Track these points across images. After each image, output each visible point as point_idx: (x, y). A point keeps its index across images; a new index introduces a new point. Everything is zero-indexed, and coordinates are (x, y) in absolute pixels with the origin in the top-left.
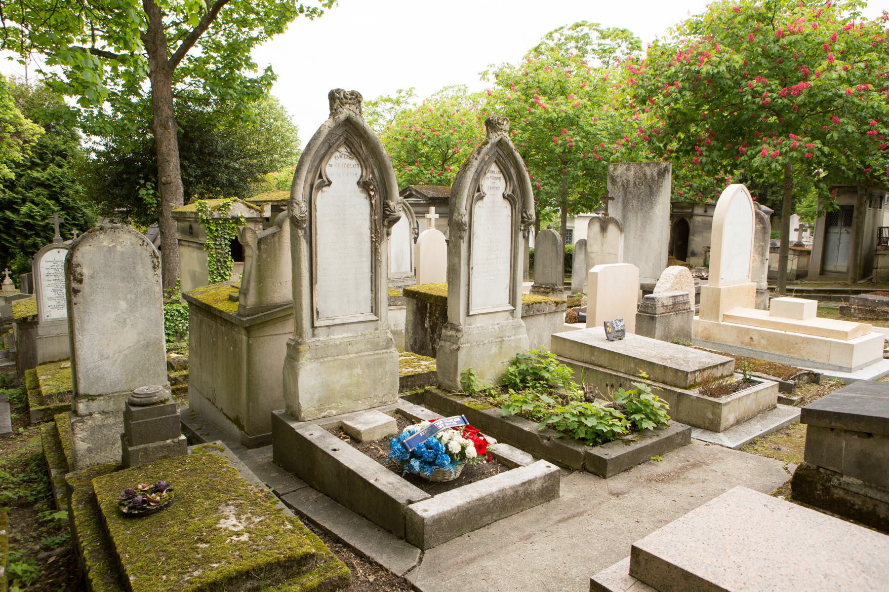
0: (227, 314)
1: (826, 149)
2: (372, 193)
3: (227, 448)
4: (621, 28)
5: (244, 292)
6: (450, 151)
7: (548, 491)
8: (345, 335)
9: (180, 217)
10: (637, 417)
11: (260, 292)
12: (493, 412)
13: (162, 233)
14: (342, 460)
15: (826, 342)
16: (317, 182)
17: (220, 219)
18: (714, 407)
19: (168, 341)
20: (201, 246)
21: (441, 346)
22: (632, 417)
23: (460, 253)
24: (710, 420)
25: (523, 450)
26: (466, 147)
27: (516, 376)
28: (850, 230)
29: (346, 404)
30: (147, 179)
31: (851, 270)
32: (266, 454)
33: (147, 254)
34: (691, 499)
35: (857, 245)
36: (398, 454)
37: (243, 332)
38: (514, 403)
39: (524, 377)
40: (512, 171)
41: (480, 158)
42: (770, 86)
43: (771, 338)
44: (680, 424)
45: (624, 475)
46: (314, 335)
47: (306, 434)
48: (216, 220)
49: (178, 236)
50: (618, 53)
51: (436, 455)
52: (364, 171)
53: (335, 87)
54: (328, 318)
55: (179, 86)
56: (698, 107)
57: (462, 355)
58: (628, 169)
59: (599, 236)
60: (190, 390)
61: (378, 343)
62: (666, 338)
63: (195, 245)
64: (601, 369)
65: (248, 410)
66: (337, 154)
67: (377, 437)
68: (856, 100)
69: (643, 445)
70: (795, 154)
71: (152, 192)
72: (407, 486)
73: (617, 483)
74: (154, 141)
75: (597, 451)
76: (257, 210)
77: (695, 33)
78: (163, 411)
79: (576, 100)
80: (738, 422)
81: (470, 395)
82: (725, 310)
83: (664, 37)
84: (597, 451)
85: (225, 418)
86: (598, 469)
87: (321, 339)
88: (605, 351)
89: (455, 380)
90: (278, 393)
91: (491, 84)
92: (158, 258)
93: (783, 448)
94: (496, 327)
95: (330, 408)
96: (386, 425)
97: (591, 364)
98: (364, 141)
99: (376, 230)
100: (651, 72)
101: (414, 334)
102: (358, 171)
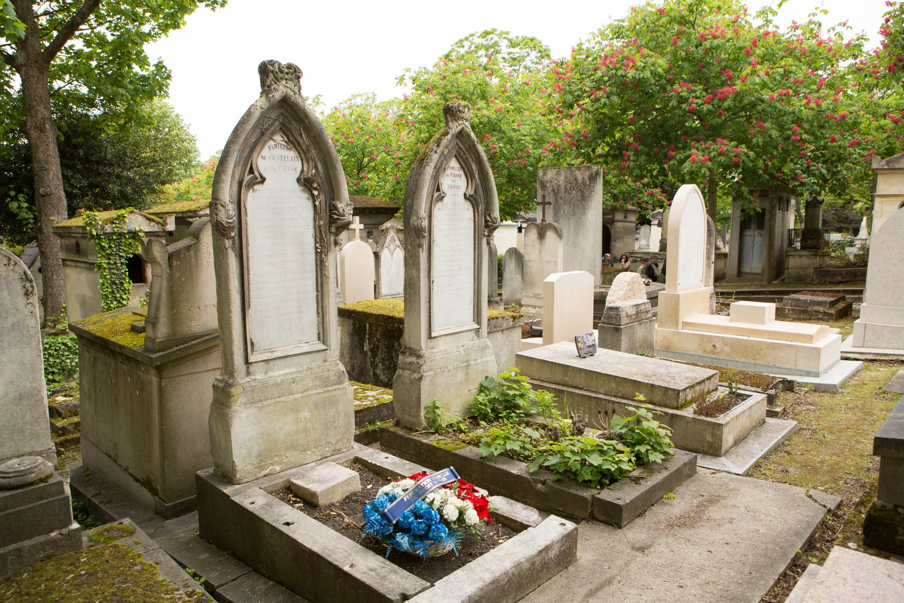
0: (130, 349)
1: (751, 154)
2: (316, 193)
3: (139, 529)
4: (530, 36)
5: (152, 320)
6: (366, 160)
7: (563, 557)
8: (288, 371)
9: (63, 233)
10: (643, 449)
11: (174, 320)
12: (469, 452)
13: (42, 253)
14: (300, 539)
15: (792, 346)
16: (247, 178)
17: (114, 233)
18: (713, 429)
19: (50, 382)
20: (91, 266)
21: (399, 376)
22: (637, 448)
23: (418, 264)
24: (709, 443)
25: (525, 503)
26: (384, 154)
27: (485, 405)
28: (762, 233)
29: (293, 456)
30: (19, 191)
31: (766, 271)
32: (188, 527)
33: (14, 276)
34: (728, 548)
35: (771, 247)
36: (377, 527)
37: (153, 372)
38: (491, 441)
39: (496, 408)
40: (474, 167)
41: (439, 150)
42: (695, 91)
43: (734, 345)
44: (683, 452)
45: (639, 521)
46: (248, 373)
47: (246, 504)
48: (109, 236)
49: (62, 255)
50: (527, 62)
51: (429, 526)
52: (306, 165)
53: (267, 58)
54: (266, 351)
55: (57, 84)
56: (624, 111)
57: (425, 385)
58: (558, 174)
59: (536, 243)
60: (82, 440)
61: (328, 378)
62: (631, 351)
63: (83, 265)
64: (577, 391)
65: (163, 470)
66: (271, 143)
67: (337, 498)
68: (778, 105)
69: (655, 483)
70: (722, 159)
71: (25, 205)
72: (396, 572)
73: (635, 532)
74: (28, 147)
75: (607, 495)
76: (158, 223)
77: (618, 37)
78: (43, 494)
79: (499, 104)
80: (737, 443)
81: (436, 432)
82: (684, 317)
83: (589, 41)
84: (607, 495)
85: (131, 479)
86: (612, 517)
87: (258, 377)
88: (580, 370)
89: (418, 415)
90: (202, 445)
91: (408, 89)
92: (31, 281)
93: (790, 470)
94: (461, 350)
95: (272, 464)
96: (347, 482)
97: (563, 385)
98: (304, 128)
99: (321, 239)
100: (578, 76)
101: (351, 358)
102: (298, 165)
